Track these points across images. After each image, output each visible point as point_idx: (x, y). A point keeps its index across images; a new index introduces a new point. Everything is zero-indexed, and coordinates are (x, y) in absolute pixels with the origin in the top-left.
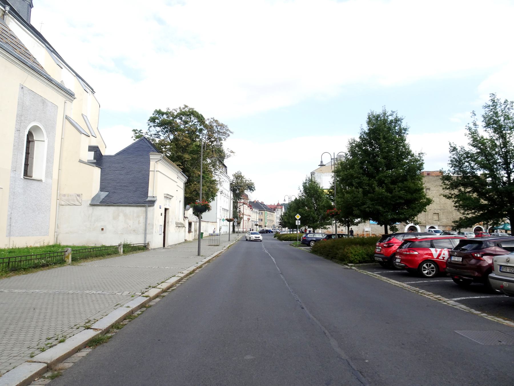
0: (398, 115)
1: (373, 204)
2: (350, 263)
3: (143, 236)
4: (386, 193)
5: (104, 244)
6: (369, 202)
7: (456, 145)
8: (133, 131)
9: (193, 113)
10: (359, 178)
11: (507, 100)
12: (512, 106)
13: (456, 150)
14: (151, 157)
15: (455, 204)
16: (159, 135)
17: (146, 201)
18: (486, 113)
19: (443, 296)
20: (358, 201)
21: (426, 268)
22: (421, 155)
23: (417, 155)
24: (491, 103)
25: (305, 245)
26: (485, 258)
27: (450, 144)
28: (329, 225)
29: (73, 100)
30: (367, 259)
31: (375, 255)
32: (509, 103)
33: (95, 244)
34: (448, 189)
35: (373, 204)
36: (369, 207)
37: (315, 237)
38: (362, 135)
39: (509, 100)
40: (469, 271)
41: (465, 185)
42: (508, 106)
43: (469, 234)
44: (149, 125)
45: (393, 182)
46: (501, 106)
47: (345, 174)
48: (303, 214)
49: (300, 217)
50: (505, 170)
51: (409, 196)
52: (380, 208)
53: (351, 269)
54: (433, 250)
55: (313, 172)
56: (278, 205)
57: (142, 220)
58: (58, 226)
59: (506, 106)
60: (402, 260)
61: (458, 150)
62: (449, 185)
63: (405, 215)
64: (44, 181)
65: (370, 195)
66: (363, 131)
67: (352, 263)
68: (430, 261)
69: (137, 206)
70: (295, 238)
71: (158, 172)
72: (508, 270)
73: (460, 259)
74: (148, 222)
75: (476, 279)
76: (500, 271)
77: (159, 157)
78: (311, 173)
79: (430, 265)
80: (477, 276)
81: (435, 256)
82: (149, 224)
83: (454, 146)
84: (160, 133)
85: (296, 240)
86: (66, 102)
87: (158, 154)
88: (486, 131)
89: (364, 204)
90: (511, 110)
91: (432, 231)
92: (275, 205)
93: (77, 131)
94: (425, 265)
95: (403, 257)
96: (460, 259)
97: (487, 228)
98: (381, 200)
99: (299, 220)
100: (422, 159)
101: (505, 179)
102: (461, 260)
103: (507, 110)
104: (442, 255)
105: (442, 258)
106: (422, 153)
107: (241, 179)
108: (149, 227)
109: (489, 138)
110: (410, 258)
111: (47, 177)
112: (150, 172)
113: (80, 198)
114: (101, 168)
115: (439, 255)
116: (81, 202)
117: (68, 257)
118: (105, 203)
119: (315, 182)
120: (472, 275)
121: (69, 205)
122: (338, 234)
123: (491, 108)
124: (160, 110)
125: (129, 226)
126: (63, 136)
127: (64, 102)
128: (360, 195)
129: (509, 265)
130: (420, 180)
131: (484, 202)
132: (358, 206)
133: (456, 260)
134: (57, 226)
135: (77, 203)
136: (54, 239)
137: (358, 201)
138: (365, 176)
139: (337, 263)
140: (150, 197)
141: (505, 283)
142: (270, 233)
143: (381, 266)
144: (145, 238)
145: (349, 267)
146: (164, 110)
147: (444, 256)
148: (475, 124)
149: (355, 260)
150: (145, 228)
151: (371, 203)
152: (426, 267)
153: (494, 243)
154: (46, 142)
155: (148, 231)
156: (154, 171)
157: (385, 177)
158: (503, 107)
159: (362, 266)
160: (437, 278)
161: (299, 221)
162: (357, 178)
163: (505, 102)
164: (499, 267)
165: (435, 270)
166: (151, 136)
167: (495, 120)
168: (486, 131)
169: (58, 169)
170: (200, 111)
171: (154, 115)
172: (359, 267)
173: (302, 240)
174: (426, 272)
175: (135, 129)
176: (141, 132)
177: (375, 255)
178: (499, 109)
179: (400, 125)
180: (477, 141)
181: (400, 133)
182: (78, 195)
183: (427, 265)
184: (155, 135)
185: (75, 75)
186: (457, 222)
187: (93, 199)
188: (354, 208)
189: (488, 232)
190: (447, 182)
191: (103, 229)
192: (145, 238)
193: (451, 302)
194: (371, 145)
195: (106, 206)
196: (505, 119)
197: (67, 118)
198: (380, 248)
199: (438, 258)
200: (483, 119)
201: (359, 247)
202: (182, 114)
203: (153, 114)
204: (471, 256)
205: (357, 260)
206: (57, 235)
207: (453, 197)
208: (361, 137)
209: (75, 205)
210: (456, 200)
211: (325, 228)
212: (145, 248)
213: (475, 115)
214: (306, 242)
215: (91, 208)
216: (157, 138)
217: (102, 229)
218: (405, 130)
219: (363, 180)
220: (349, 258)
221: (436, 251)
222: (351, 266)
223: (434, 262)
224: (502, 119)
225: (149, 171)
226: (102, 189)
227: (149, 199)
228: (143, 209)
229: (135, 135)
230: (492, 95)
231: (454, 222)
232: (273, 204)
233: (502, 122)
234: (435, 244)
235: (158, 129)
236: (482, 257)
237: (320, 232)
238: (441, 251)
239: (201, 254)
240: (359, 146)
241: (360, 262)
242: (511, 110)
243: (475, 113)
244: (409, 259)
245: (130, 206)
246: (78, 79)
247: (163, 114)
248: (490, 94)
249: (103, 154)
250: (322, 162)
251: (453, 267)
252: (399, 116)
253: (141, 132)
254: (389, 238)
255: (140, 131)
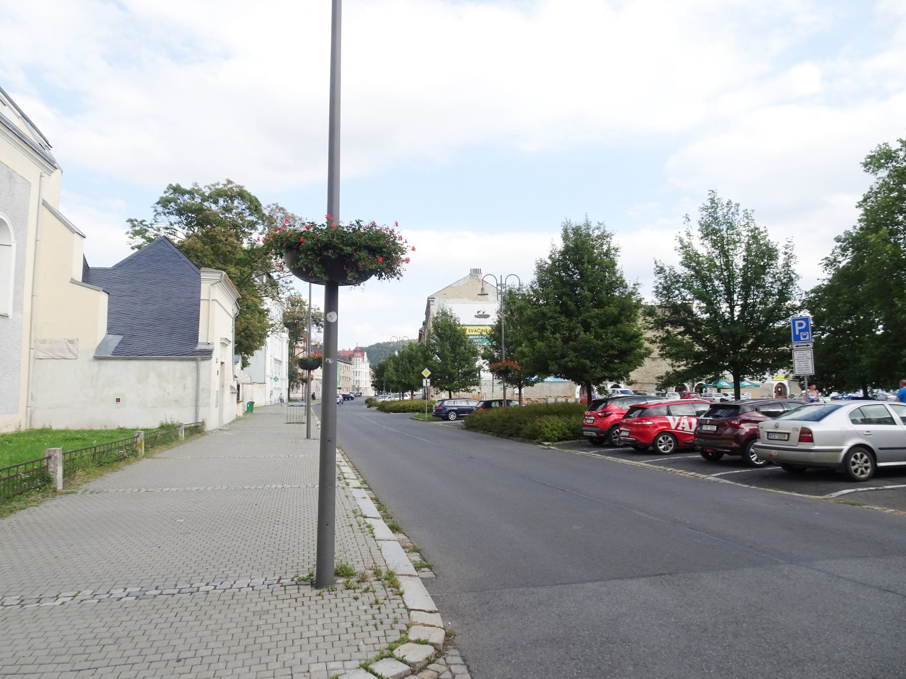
0: (606, 229)
1: (576, 357)
2: (545, 441)
3: (192, 409)
4: (595, 341)
5: (122, 426)
6: (572, 354)
7: (664, 264)
8: (127, 221)
9: (242, 195)
10: (555, 319)
11: (730, 201)
12: (737, 211)
13: (664, 272)
14: (204, 276)
15: (660, 351)
16: (173, 230)
17: (196, 351)
18: (703, 218)
19: (698, 473)
20: (556, 352)
21: (662, 442)
22: (636, 286)
23: (632, 286)
24: (709, 204)
25: (438, 418)
26: (742, 425)
27: (656, 263)
28: (474, 385)
29: (52, 170)
30: (569, 435)
31: (584, 428)
32: (733, 205)
33: (105, 426)
34: (651, 329)
35: (576, 357)
36: (571, 361)
37: (456, 405)
38: (554, 254)
39: (734, 202)
40: (724, 441)
41: (674, 324)
42: (732, 210)
43: (672, 396)
44: (156, 211)
45: (603, 325)
46: (723, 209)
47: (534, 313)
48: (434, 368)
49: (430, 373)
50: (728, 302)
51: (624, 346)
52: (587, 362)
53: (549, 449)
54: (670, 418)
55: (433, 297)
56: (356, 351)
57: (190, 382)
58: (32, 396)
59: (729, 210)
60: (631, 433)
61: (667, 272)
62: (652, 323)
63: (619, 372)
64: (10, 318)
65: (573, 343)
66: (555, 248)
67: (548, 441)
68: (667, 432)
69: (181, 360)
70: (411, 408)
71: (215, 302)
72: (777, 437)
73: (714, 428)
74: (201, 386)
75: (734, 451)
76: (768, 438)
77: (218, 277)
78: (428, 298)
79: (667, 438)
80: (735, 448)
81: (673, 426)
82: (202, 390)
83: (661, 266)
84: (176, 226)
85: (424, 412)
86: (43, 174)
87: (216, 271)
88: (703, 244)
89: (563, 356)
90: (736, 215)
91: (618, 392)
92: (350, 351)
93: (63, 226)
94: (661, 439)
95: (634, 430)
96: (714, 428)
97: (693, 386)
98: (586, 351)
99: (428, 378)
100: (638, 292)
101: (727, 315)
102: (715, 430)
103: (731, 216)
104: (681, 425)
105: (681, 429)
106: (638, 284)
107: (301, 306)
108: (202, 395)
109: (706, 254)
110: (642, 430)
111: (14, 310)
112: (202, 302)
113: (74, 346)
114: (108, 294)
115: (678, 425)
116: (76, 353)
117: (140, 446)
118: (123, 353)
119: (451, 317)
120: (729, 446)
121: (53, 358)
122: (508, 400)
123: (710, 210)
124: (178, 186)
125: (166, 393)
126: (39, 236)
127: (39, 175)
128: (559, 343)
129: (778, 431)
130: (634, 321)
131: (698, 348)
132: (555, 359)
133: (709, 429)
134: (31, 397)
135: (69, 355)
136: (26, 420)
137: (556, 352)
138: (563, 315)
139: (522, 441)
140: (202, 343)
141: (773, 452)
142: (348, 400)
143: (590, 443)
144: (197, 413)
145: (546, 447)
146: (187, 186)
147: (683, 426)
148: (688, 234)
149: (553, 437)
150: (831, 409)
151: (575, 355)
152: (663, 441)
153: (751, 407)
154: (14, 246)
155: (200, 401)
156: (209, 300)
157: (592, 318)
158: (725, 211)
159: (563, 444)
160: (677, 455)
161: (429, 380)
162: (551, 318)
163: (727, 204)
164: (766, 434)
165: (673, 444)
166: (159, 230)
167: (714, 229)
168: (703, 244)
169: (31, 295)
170: (252, 189)
171: (167, 194)
172: (558, 446)
173: (434, 411)
174: (662, 447)
175: (133, 218)
176: (144, 223)
177: (584, 428)
178: (720, 214)
179: (609, 243)
180: (690, 259)
181: (607, 254)
182: (71, 342)
183: (664, 438)
184: (167, 228)
185: (20, 115)
186: (662, 377)
187: (99, 348)
188: (549, 362)
189: (694, 391)
190: (649, 319)
191: (119, 399)
192: (197, 413)
193: (712, 478)
194: (566, 268)
195: (124, 359)
196: (727, 229)
197: (45, 204)
198: (593, 418)
199: (676, 429)
200: (699, 227)
201: (556, 418)
202: (216, 195)
203: (165, 192)
204: (727, 424)
205: (556, 437)
206: (32, 412)
207: (658, 341)
208: (550, 256)
209: (65, 358)
210: (661, 345)
211: (468, 391)
212: (196, 430)
213: (689, 220)
214: (442, 414)
215: (96, 363)
216: (171, 234)
217: (118, 400)
218: (616, 250)
219: (562, 322)
220: (544, 434)
221: (674, 420)
222: (548, 445)
223: (672, 434)
224: (724, 227)
225: (199, 300)
226: (111, 330)
227: (200, 347)
228: (192, 364)
229: (133, 229)
230: (711, 192)
231: (658, 378)
232: (347, 349)
233: (724, 233)
234: (672, 412)
235: (174, 218)
236: (740, 424)
237: (290, 394)
238: (680, 420)
239: (311, 435)
240: (550, 271)
241: (560, 440)
242: (736, 215)
243: (689, 217)
244: (641, 432)
245: (169, 359)
246: (24, 122)
247: (183, 192)
248: (709, 191)
249: (90, 266)
250: (482, 289)
251: (706, 438)
252: (609, 230)
253: (144, 223)
254: (604, 404)
255: (141, 222)
